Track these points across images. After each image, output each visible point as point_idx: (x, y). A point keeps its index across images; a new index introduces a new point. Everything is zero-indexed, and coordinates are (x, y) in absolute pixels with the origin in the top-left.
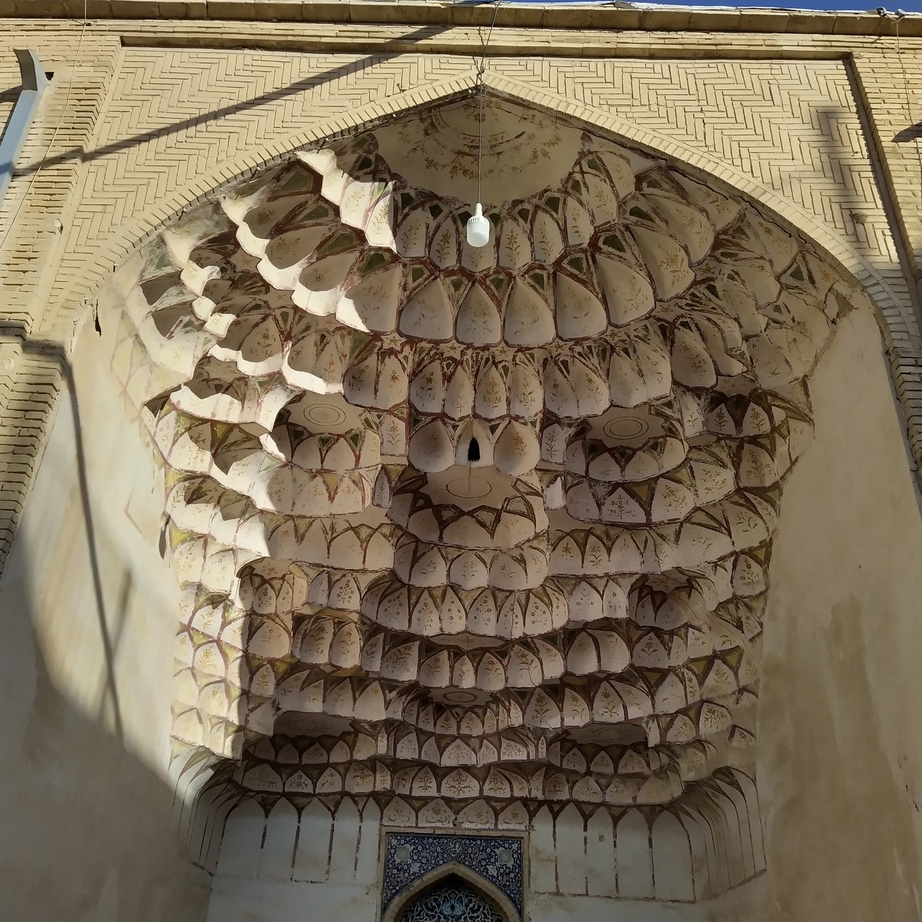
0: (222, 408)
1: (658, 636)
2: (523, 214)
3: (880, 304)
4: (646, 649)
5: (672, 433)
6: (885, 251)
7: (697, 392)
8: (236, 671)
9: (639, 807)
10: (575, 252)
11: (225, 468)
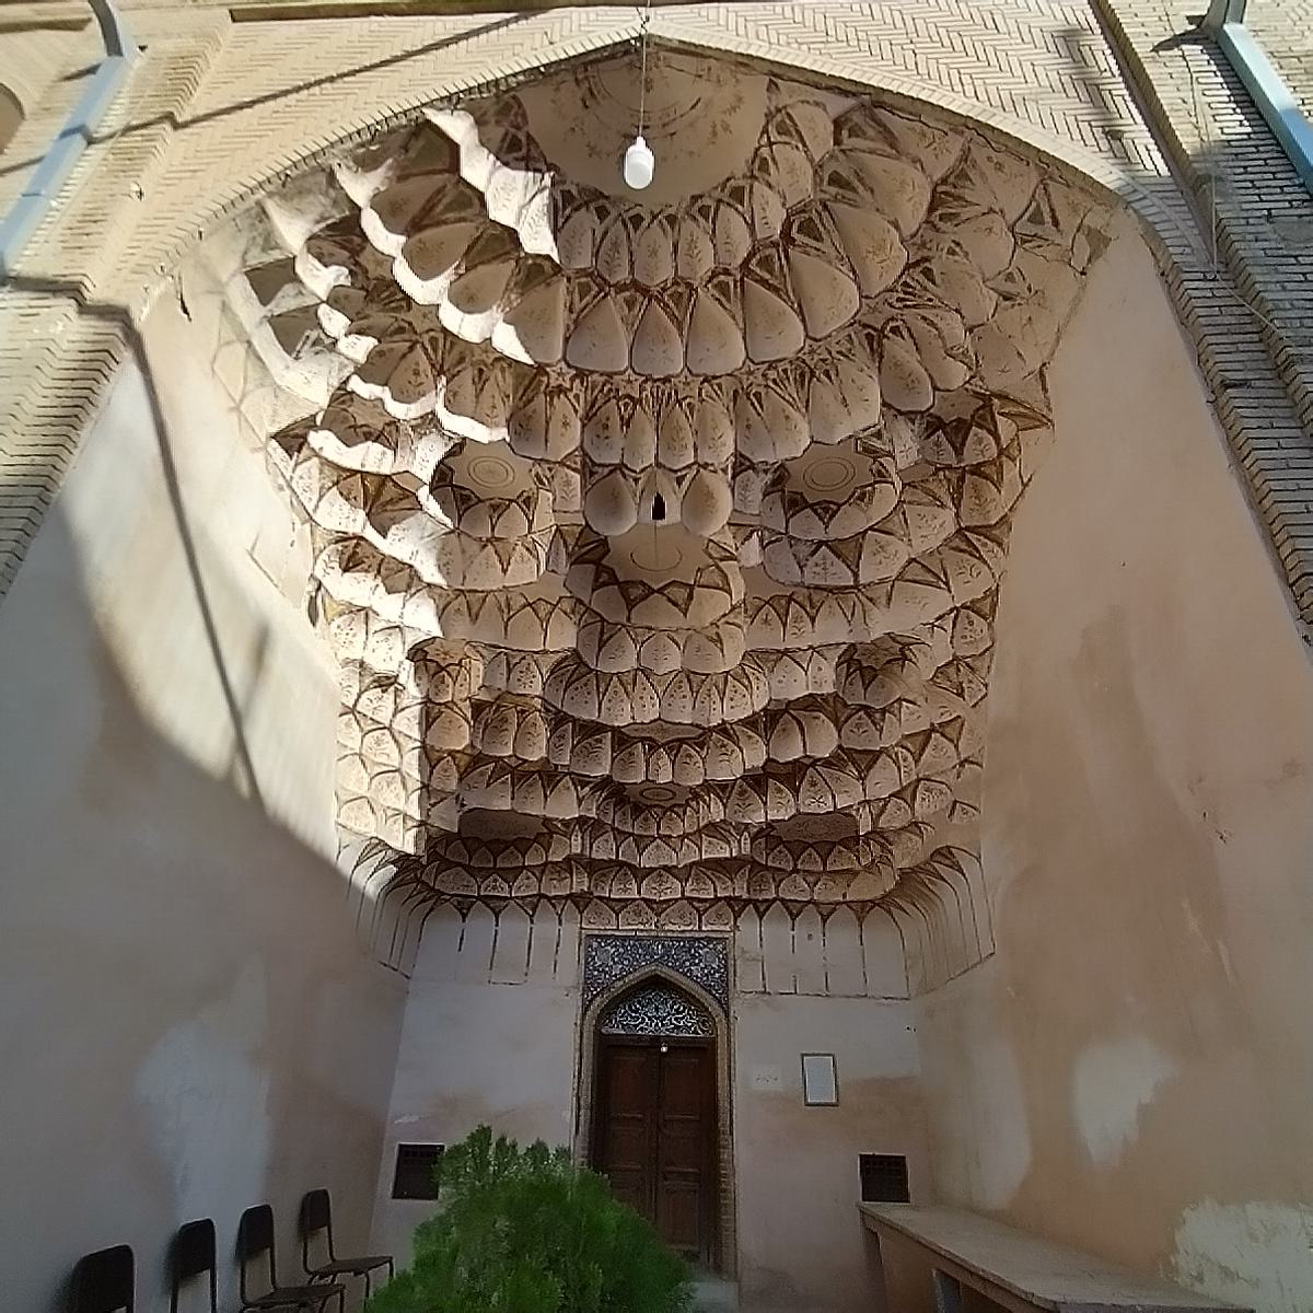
0: (370, 457)
2: (704, 211)
3: (1150, 219)
4: (856, 730)
5: (882, 476)
6: (1154, 162)
7: (910, 416)
8: (415, 763)
10: (766, 247)
11: (383, 533)
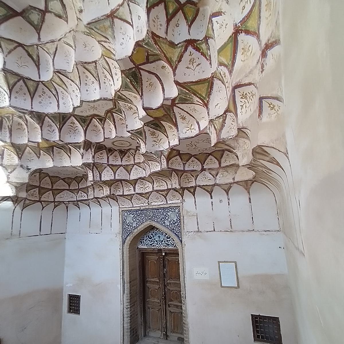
9: (237, 183)
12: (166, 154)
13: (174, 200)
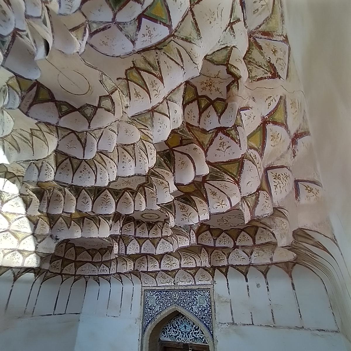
1: (228, 135)
4: (221, 148)
9: (276, 264)
12: (196, 228)
13: (203, 281)
